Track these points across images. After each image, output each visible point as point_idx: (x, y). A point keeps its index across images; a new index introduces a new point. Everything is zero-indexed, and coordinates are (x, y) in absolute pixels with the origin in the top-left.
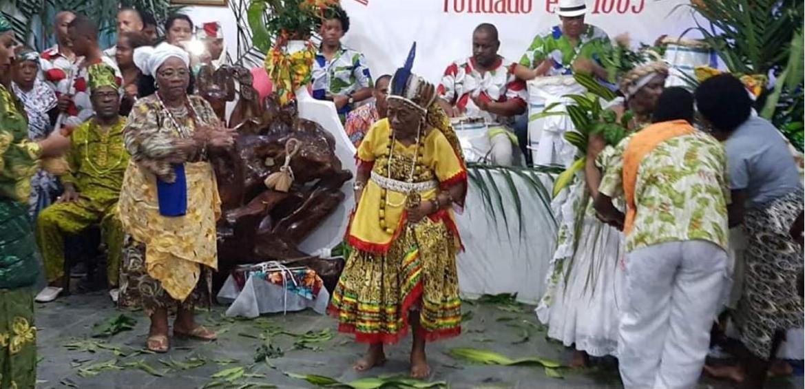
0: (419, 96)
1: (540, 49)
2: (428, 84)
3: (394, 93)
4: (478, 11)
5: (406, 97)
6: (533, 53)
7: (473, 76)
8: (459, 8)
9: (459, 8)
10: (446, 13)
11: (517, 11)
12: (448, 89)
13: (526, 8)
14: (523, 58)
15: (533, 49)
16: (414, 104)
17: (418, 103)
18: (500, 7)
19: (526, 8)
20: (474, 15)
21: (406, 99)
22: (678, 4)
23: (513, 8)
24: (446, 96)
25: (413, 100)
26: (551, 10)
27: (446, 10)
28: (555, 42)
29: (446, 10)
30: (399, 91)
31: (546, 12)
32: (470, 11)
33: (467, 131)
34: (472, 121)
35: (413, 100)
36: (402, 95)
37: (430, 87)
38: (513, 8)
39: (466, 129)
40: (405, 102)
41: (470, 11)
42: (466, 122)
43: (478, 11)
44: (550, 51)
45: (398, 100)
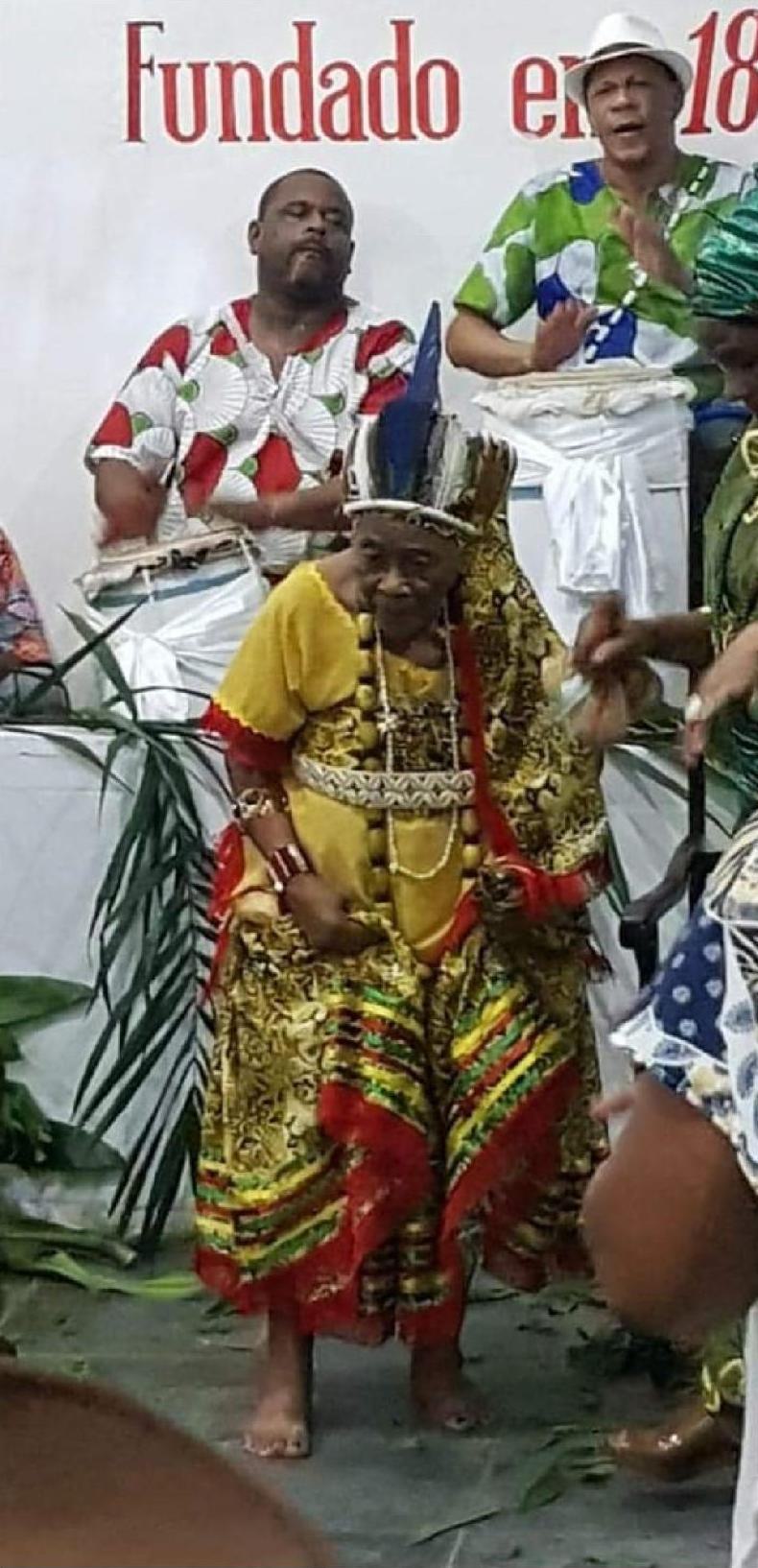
0: (471, 493)
1: (521, 236)
2: (494, 447)
3: (381, 490)
4: (259, 134)
5: (429, 503)
6: (502, 251)
7: (243, 364)
8: (186, 124)
9: (186, 124)
10: (133, 145)
11: (405, 133)
12: (146, 423)
13: (438, 121)
14: (470, 281)
15: (500, 243)
16: (458, 521)
17: (466, 518)
18: (341, 122)
19: (438, 121)
20: (245, 150)
21: (428, 510)
22: (655, 24)
23: (390, 122)
24: (135, 449)
25: (452, 510)
26: (534, 121)
27: (134, 134)
28: (577, 216)
29: (134, 134)
30: (400, 479)
31: (516, 133)
32: (229, 134)
33: (168, 603)
34: (182, 563)
35: (452, 510)
36: (415, 499)
37: (499, 453)
38: (390, 122)
39: (157, 595)
40: (426, 518)
41: (229, 134)
42: (158, 569)
43: (259, 134)
44: (553, 249)
45: (401, 514)
